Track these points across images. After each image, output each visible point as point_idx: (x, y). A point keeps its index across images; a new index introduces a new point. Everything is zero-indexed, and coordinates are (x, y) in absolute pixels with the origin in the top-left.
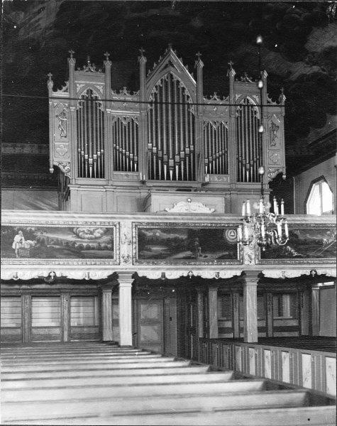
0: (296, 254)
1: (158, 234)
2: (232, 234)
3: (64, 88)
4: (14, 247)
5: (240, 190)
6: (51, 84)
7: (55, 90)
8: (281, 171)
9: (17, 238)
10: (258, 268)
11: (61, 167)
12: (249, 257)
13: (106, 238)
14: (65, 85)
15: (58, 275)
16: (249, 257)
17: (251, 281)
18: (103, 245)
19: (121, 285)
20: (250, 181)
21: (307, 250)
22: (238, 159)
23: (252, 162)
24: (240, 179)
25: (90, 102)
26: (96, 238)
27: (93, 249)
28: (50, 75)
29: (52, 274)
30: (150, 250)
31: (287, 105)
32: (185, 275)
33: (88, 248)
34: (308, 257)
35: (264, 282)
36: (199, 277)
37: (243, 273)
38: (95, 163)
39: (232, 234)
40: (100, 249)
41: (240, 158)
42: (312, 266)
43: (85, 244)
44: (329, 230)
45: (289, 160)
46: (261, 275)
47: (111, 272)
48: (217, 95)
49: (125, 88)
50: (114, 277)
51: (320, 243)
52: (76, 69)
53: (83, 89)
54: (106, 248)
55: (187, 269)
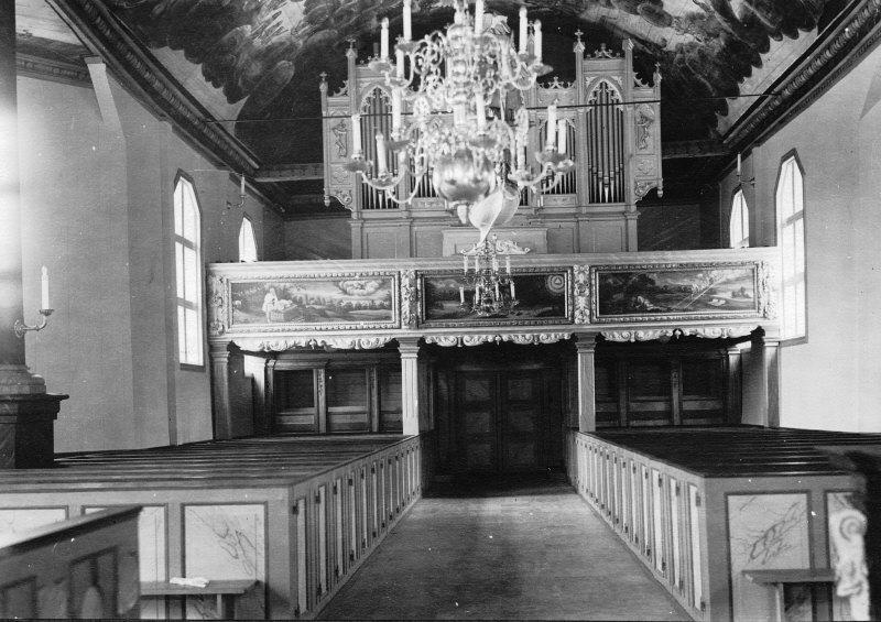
0: (650, 306)
1: (452, 286)
2: (558, 281)
3: (343, 90)
4: (264, 309)
5: (593, 214)
6: (323, 87)
7: (330, 94)
8: (654, 184)
9: (269, 297)
10: (419, 333)
11: (339, 198)
12: (582, 308)
13: (382, 293)
14: (344, 86)
15: (687, 332)
16: (582, 308)
17: (586, 347)
18: (377, 303)
19: (403, 355)
20: (610, 201)
21: (668, 300)
22: (591, 170)
23: (612, 173)
24: (595, 198)
25: (603, 103)
26: (370, 294)
27: (365, 308)
28: (323, 75)
29: (678, 333)
30: (442, 307)
31: (665, 88)
32: (490, 339)
33: (359, 307)
34: (669, 310)
35: (429, 353)
36: (510, 343)
37: (573, 335)
38: (612, 182)
39: (558, 281)
40: (372, 308)
41: (595, 169)
42: (310, 333)
43: (354, 303)
44: (701, 271)
45: (668, 168)
46: (600, 338)
47: (754, 328)
48: (559, 80)
49: (556, 78)
50: (393, 347)
51: (686, 291)
52: (585, 57)
53: (594, 82)
54: (382, 307)
55: (491, 333)
